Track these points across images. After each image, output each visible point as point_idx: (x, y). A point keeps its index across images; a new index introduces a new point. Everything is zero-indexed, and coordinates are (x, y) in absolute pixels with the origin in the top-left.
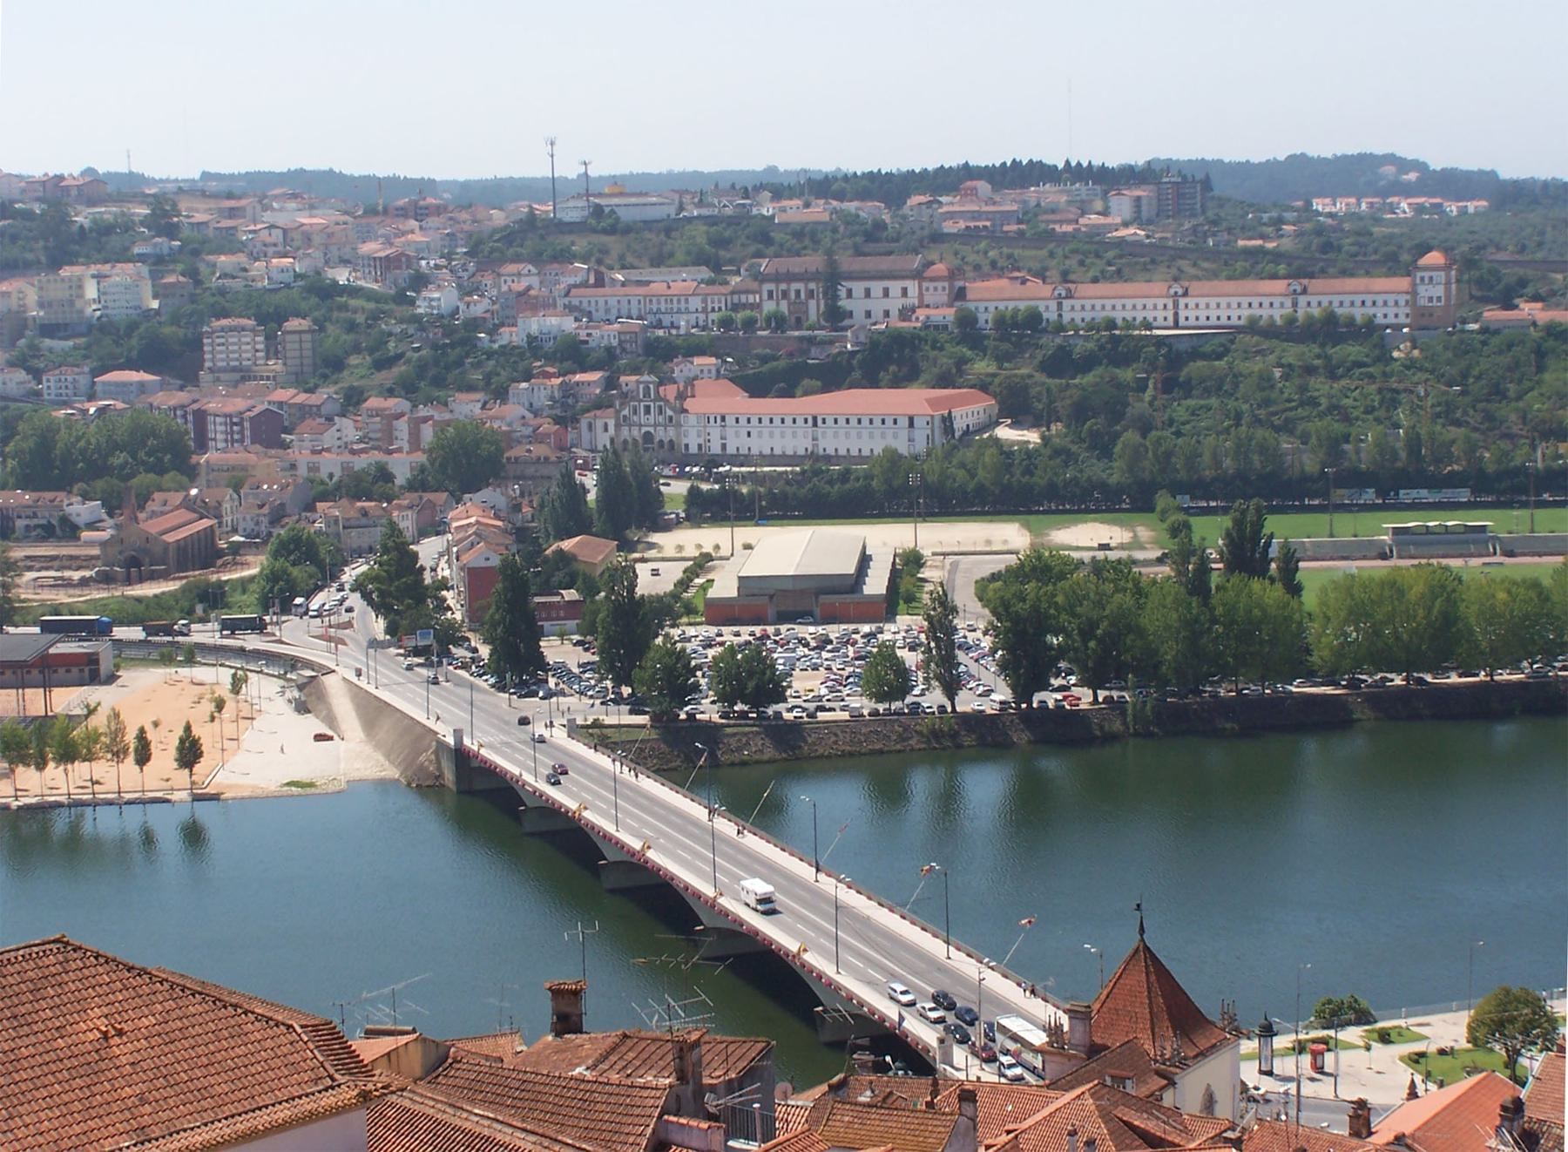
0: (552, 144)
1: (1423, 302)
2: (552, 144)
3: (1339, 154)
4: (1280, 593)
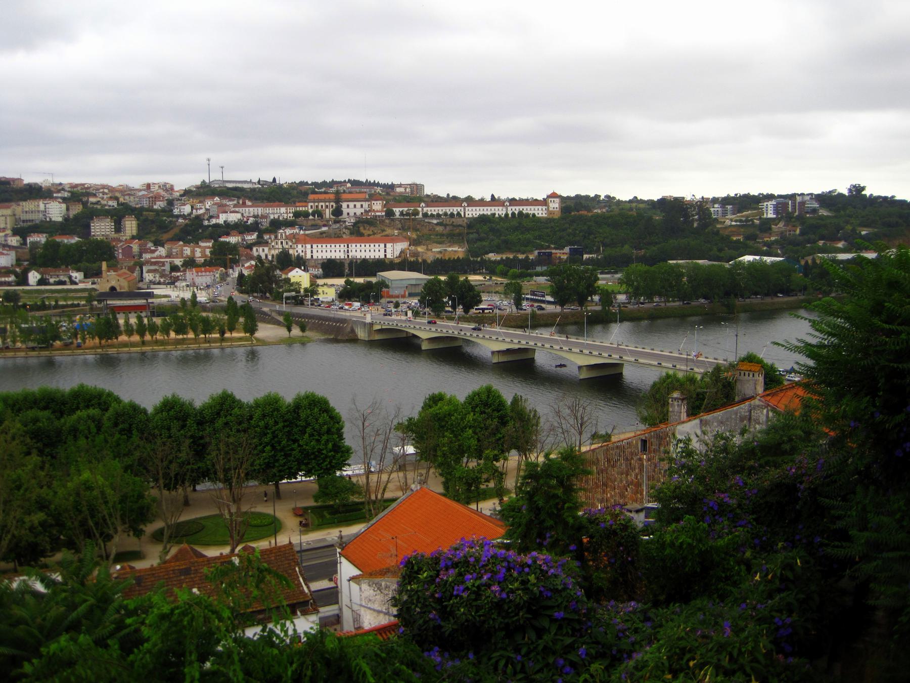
0: (209, 160)
1: (551, 209)
2: (209, 160)
3: (732, 195)
4: (517, 458)
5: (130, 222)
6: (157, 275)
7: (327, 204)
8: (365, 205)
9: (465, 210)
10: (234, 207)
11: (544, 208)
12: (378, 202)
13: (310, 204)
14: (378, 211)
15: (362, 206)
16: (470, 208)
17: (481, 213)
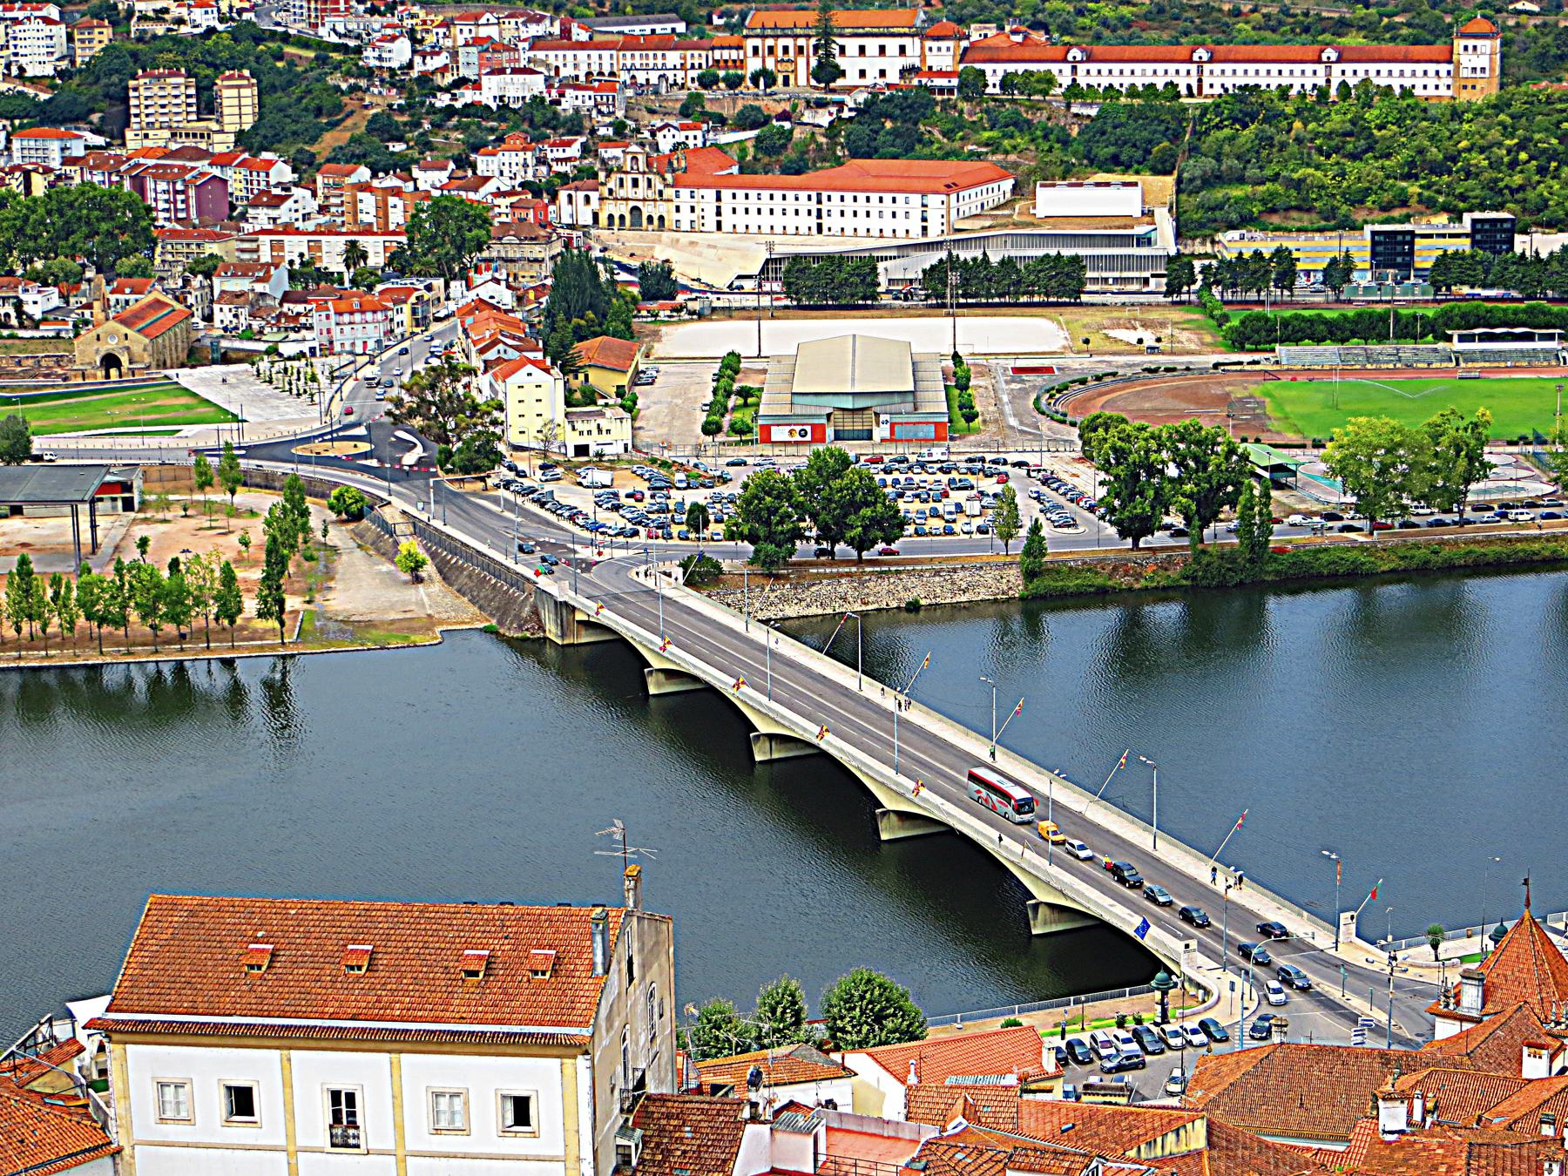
1: (1465, 73)
5: (234, 92)
6: (244, 312)
7: (801, 42)
8: (913, 45)
9: (1200, 72)
10: (532, 48)
11: (1444, 68)
12: (944, 44)
13: (750, 44)
14: (941, 74)
15: (902, 49)
16: (1217, 67)
17: (1241, 81)
